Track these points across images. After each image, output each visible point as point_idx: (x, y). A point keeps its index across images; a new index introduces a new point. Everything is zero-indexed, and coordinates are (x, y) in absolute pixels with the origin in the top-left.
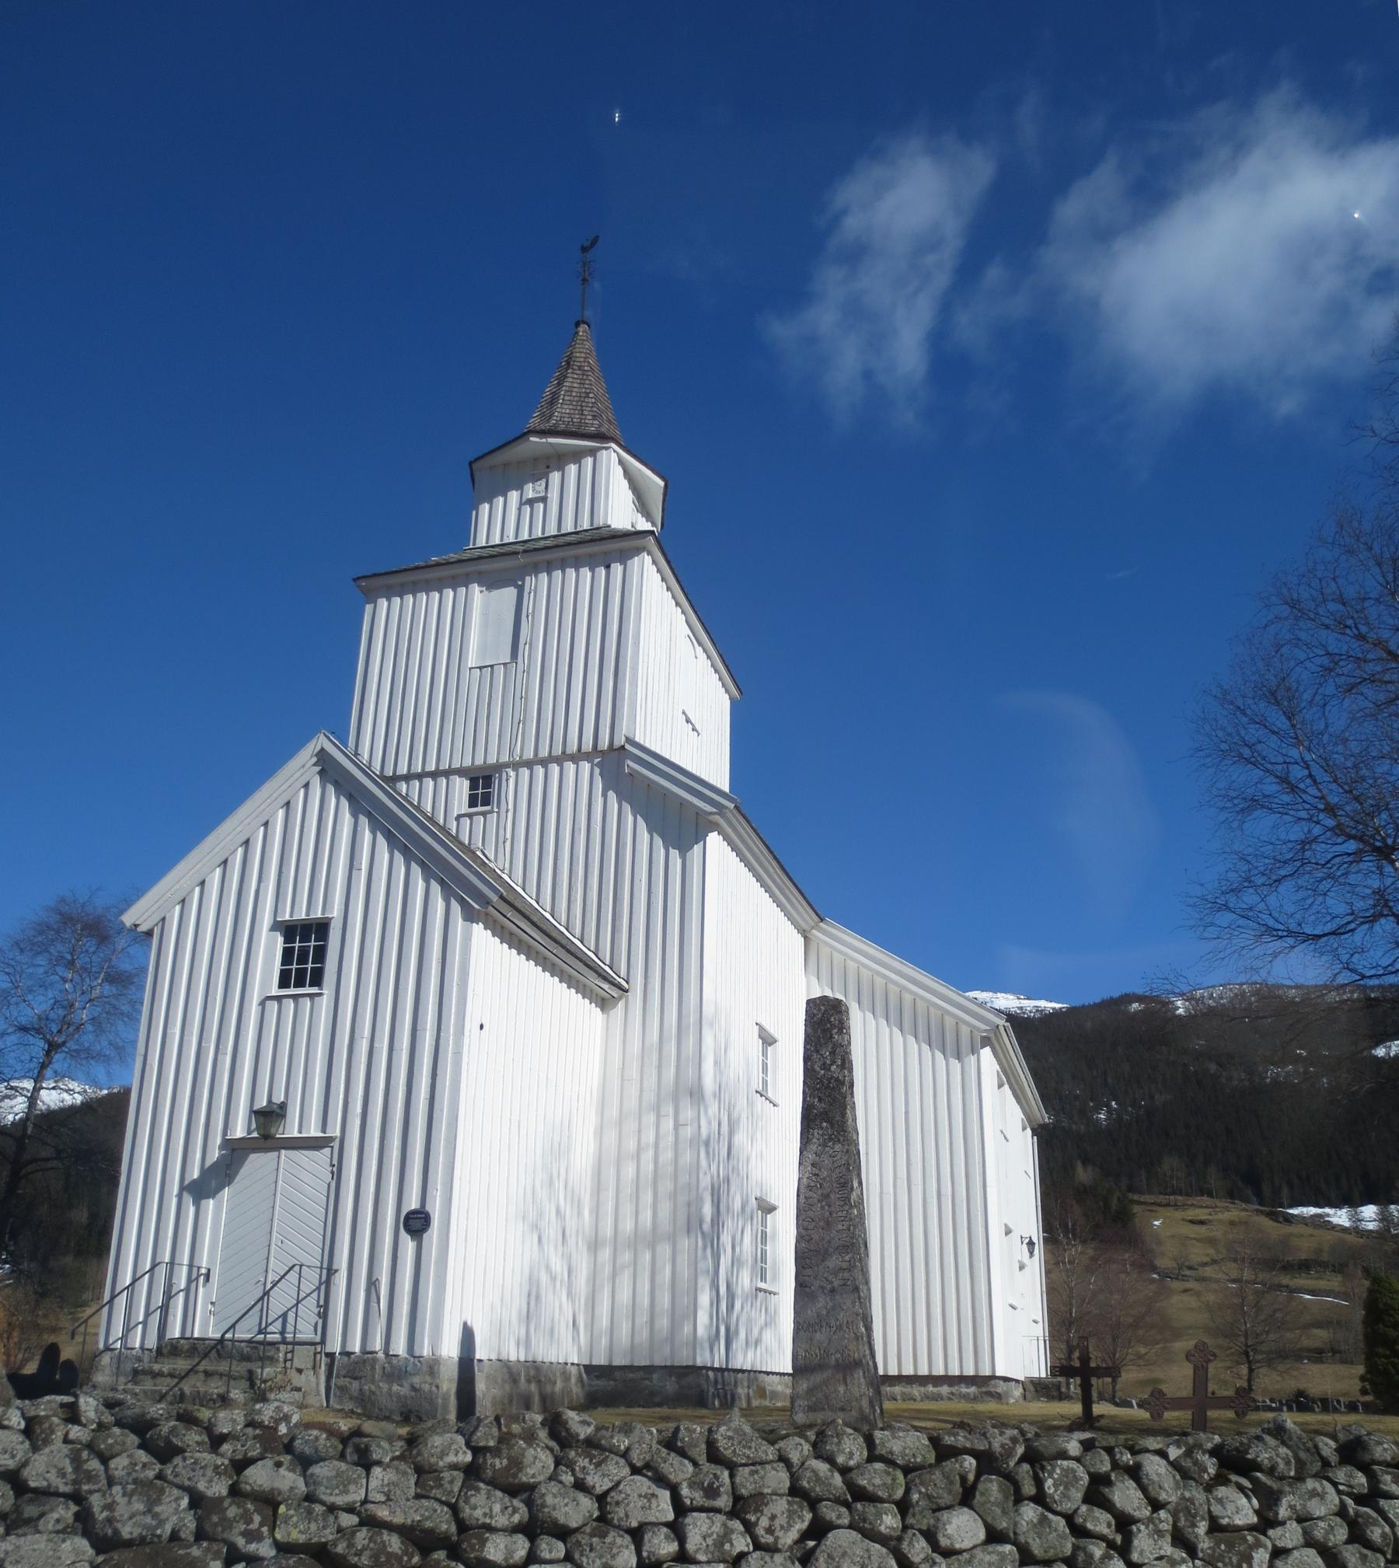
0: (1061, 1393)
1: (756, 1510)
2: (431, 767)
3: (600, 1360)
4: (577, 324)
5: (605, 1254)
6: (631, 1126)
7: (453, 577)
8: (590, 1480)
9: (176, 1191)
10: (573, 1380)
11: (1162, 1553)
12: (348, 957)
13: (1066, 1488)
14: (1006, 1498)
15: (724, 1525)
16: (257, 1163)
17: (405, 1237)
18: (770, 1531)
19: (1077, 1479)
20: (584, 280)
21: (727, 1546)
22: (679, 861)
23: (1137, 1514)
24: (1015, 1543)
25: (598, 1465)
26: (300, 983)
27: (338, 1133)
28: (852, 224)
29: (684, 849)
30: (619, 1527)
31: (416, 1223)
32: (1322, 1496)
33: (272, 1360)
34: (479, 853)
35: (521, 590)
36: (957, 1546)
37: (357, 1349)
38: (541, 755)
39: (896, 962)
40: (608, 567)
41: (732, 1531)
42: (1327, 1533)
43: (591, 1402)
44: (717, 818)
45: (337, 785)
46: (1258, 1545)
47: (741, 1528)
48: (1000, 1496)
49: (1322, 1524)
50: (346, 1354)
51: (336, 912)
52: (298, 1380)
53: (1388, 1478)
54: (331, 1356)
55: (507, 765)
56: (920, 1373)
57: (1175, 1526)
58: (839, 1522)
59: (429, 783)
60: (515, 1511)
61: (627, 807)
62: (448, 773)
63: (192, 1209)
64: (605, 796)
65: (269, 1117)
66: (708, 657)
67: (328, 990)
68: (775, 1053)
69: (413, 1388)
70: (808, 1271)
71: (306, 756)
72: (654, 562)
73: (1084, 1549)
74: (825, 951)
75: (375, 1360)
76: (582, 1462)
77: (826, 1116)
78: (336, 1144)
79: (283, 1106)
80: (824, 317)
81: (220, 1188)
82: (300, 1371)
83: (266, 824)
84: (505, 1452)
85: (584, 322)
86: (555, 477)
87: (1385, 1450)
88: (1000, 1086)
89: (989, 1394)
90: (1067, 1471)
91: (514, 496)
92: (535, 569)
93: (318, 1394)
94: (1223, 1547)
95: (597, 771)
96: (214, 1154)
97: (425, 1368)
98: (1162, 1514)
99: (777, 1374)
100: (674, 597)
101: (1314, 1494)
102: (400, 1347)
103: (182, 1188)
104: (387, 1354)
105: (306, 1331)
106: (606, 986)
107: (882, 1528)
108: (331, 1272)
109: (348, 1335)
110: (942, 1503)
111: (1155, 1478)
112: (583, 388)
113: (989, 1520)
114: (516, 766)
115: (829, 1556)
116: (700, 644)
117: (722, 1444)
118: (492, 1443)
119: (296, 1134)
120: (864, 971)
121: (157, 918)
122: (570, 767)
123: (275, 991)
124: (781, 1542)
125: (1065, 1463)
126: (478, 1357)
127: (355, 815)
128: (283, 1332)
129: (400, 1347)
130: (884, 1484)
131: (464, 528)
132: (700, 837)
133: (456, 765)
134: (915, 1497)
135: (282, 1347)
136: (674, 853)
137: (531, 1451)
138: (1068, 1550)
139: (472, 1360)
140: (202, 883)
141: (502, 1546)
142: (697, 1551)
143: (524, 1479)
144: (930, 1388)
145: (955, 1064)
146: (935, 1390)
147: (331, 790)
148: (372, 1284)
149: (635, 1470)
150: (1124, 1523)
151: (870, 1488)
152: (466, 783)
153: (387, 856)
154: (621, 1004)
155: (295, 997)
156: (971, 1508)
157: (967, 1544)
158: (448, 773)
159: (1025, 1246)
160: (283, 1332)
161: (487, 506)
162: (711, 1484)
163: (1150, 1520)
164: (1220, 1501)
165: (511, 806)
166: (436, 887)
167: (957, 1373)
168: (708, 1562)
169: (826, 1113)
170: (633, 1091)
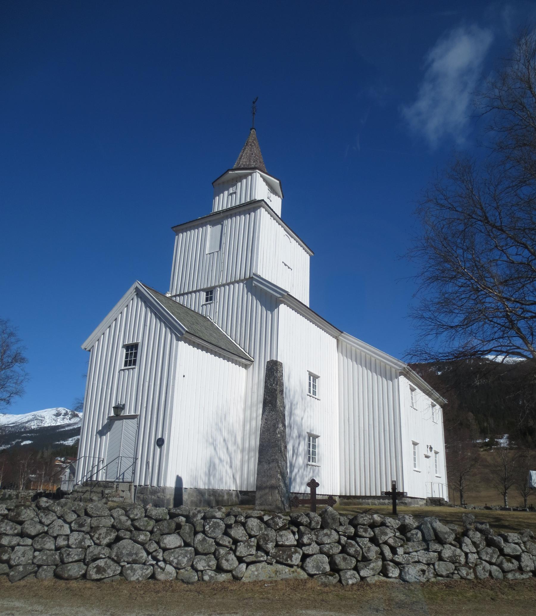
0: (440, 503)
1: (94, 532)
2: (186, 291)
3: (244, 489)
4: (251, 130)
5: (246, 452)
6: (254, 409)
7: (202, 224)
8: (43, 520)
9: (95, 434)
10: (234, 496)
11: (251, 553)
12: (143, 355)
13: (214, 529)
14: (191, 531)
15: (83, 536)
16: (117, 423)
17: (157, 447)
18: (98, 539)
19: (219, 526)
20: (254, 113)
21: (83, 543)
22: (270, 315)
23: (240, 539)
24: (194, 547)
25: (46, 515)
26: (130, 365)
27: (139, 413)
28: (437, 66)
29: (272, 311)
30: (51, 536)
31: (160, 442)
32: (329, 536)
33: (112, 487)
34: (208, 317)
35: (222, 225)
36: (168, 547)
37: (143, 484)
38: (228, 282)
39: (368, 346)
40: (249, 214)
41: (85, 538)
42: (329, 549)
43: (242, 503)
44: (282, 299)
45: (141, 298)
46: (296, 552)
47: (89, 537)
48: (189, 531)
49: (327, 546)
50: (140, 486)
51: (140, 341)
52: (122, 494)
53: (362, 530)
54: (135, 486)
55: (217, 286)
56: (377, 495)
57: (258, 543)
58: (125, 537)
59: (194, 294)
60: (16, 529)
61: (254, 298)
62: (199, 291)
63: (99, 439)
64: (247, 294)
65: (119, 408)
66: (297, 242)
67: (137, 367)
68: (319, 381)
69: (158, 497)
70: (262, 457)
71: (132, 290)
72: (266, 210)
73: (218, 550)
74: (344, 344)
75: (147, 488)
76: (42, 514)
77: (270, 402)
78: (138, 417)
79: (124, 405)
80: (423, 104)
81: (107, 433)
82: (123, 491)
83: (121, 313)
84: (15, 510)
85: (253, 128)
86: (239, 184)
87: (364, 520)
88: (412, 390)
89: (402, 503)
90: (215, 523)
91: (226, 193)
92: (227, 218)
93: (131, 498)
94: (281, 552)
95: (245, 286)
96: (106, 421)
97: (161, 491)
98: (253, 539)
99: (321, 495)
100: (277, 222)
101: (326, 535)
102: (155, 484)
103: (97, 433)
104: (151, 486)
105: (128, 477)
106: (244, 360)
107: (139, 540)
108: (136, 459)
109: (140, 480)
110: (164, 532)
111: (251, 526)
112: (252, 151)
113: (184, 539)
114: (220, 286)
115: (118, 548)
116: (292, 237)
117: (89, 510)
118: (12, 508)
119: (128, 414)
120: (358, 350)
121: (91, 346)
122: (237, 285)
123: (123, 368)
124: (102, 542)
125: (215, 520)
126: (184, 486)
127: (146, 308)
128: (123, 479)
129: (155, 484)
130: (144, 525)
131: (211, 205)
132: (277, 306)
133: (202, 288)
134: (155, 530)
135: (115, 483)
136: (269, 312)
137: (25, 510)
138: (213, 550)
139: (182, 488)
140: (104, 334)
141: (8, 540)
142: (72, 544)
143: (21, 519)
144: (381, 501)
145: (390, 383)
146: (383, 501)
147: (139, 300)
148: (148, 463)
149: (59, 518)
150: (236, 542)
151: (138, 526)
152: (205, 294)
153: (155, 320)
154: (251, 366)
155: (128, 369)
156: (179, 534)
157: (172, 546)
158: (199, 291)
159: (429, 449)
160: (123, 479)
161: (218, 197)
162: (82, 523)
163: (247, 541)
164: (281, 536)
165: (218, 301)
166: (168, 330)
167: (354, 495)
168: (76, 548)
169: (270, 401)
170: (255, 396)
